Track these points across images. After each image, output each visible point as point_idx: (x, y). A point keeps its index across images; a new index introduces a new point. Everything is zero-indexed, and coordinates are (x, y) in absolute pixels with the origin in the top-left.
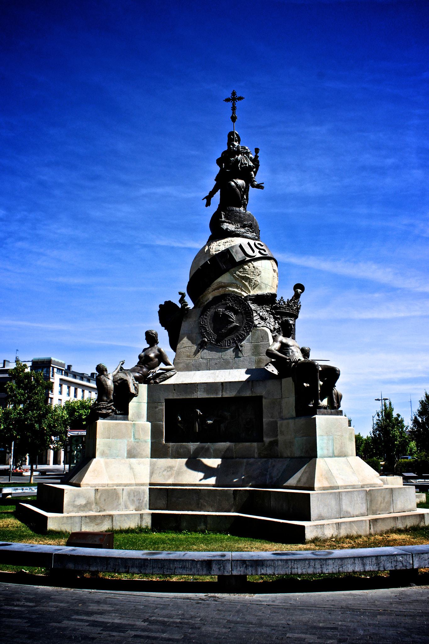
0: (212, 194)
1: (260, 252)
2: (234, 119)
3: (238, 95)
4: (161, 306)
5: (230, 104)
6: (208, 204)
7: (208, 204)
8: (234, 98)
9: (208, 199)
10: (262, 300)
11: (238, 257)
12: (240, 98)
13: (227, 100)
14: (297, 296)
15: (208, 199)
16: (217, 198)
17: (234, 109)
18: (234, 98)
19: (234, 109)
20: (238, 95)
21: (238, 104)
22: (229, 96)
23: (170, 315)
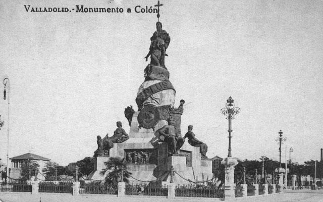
0: (148, 56)
2: (65, 10)
3: (161, 3)
4: (246, 159)
6: (147, 60)
7: (147, 60)
10: (164, 107)
11: (155, 88)
12: (162, 5)
14: (181, 105)
15: (147, 58)
16: (149, 59)
20: (161, 3)
23: (129, 113)
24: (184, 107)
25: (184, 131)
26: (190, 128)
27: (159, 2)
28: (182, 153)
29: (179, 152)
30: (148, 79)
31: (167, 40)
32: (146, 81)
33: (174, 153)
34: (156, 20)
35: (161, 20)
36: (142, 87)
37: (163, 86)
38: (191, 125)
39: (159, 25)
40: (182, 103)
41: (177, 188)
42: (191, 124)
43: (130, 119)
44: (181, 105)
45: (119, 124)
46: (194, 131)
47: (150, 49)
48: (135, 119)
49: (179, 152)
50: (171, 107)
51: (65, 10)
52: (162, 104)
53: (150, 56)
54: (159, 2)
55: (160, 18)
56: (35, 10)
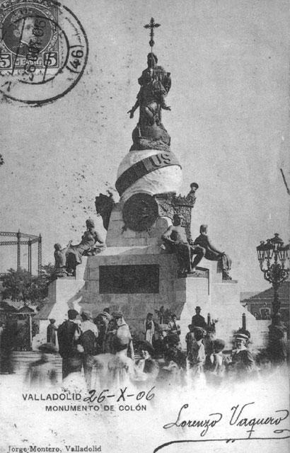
0: (134, 109)
1: (165, 162)
2: (152, 43)
3: (155, 22)
5: (149, 30)
6: (132, 116)
7: (132, 116)
8: (152, 25)
9: (132, 112)
10: (163, 196)
13: (147, 27)
14: (192, 192)
16: (137, 113)
17: (152, 35)
18: (152, 25)
19: (152, 35)
20: (155, 22)
21: (155, 30)
22: (148, 23)
23: (104, 205)
24: (196, 194)
25: (195, 234)
26: (203, 229)
27: (152, 20)
28: (199, 271)
29: (194, 270)
30: (137, 146)
31: (167, 82)
32: (133, 149)
33: (189, 272)
34: (148, 50)
35: (155, 52)
36: (126, 161)
37: (162, 160)
38: (205, 224)
39: (152, 59)
40: (194, 188)
41: (157, 338)
42: (205, 223)
43: (106, 217)
44: (192, 192)
45: (90, 225)
46: (208, 234)
47: (139, 83)
48: (116, 215)
49: (194, 270)
50: (177, 195)
51: (152, 43)
52: (160, 191)
53: (139, 108)
54: (152, 20)
55: (153, 47)
56: (34, 398)
